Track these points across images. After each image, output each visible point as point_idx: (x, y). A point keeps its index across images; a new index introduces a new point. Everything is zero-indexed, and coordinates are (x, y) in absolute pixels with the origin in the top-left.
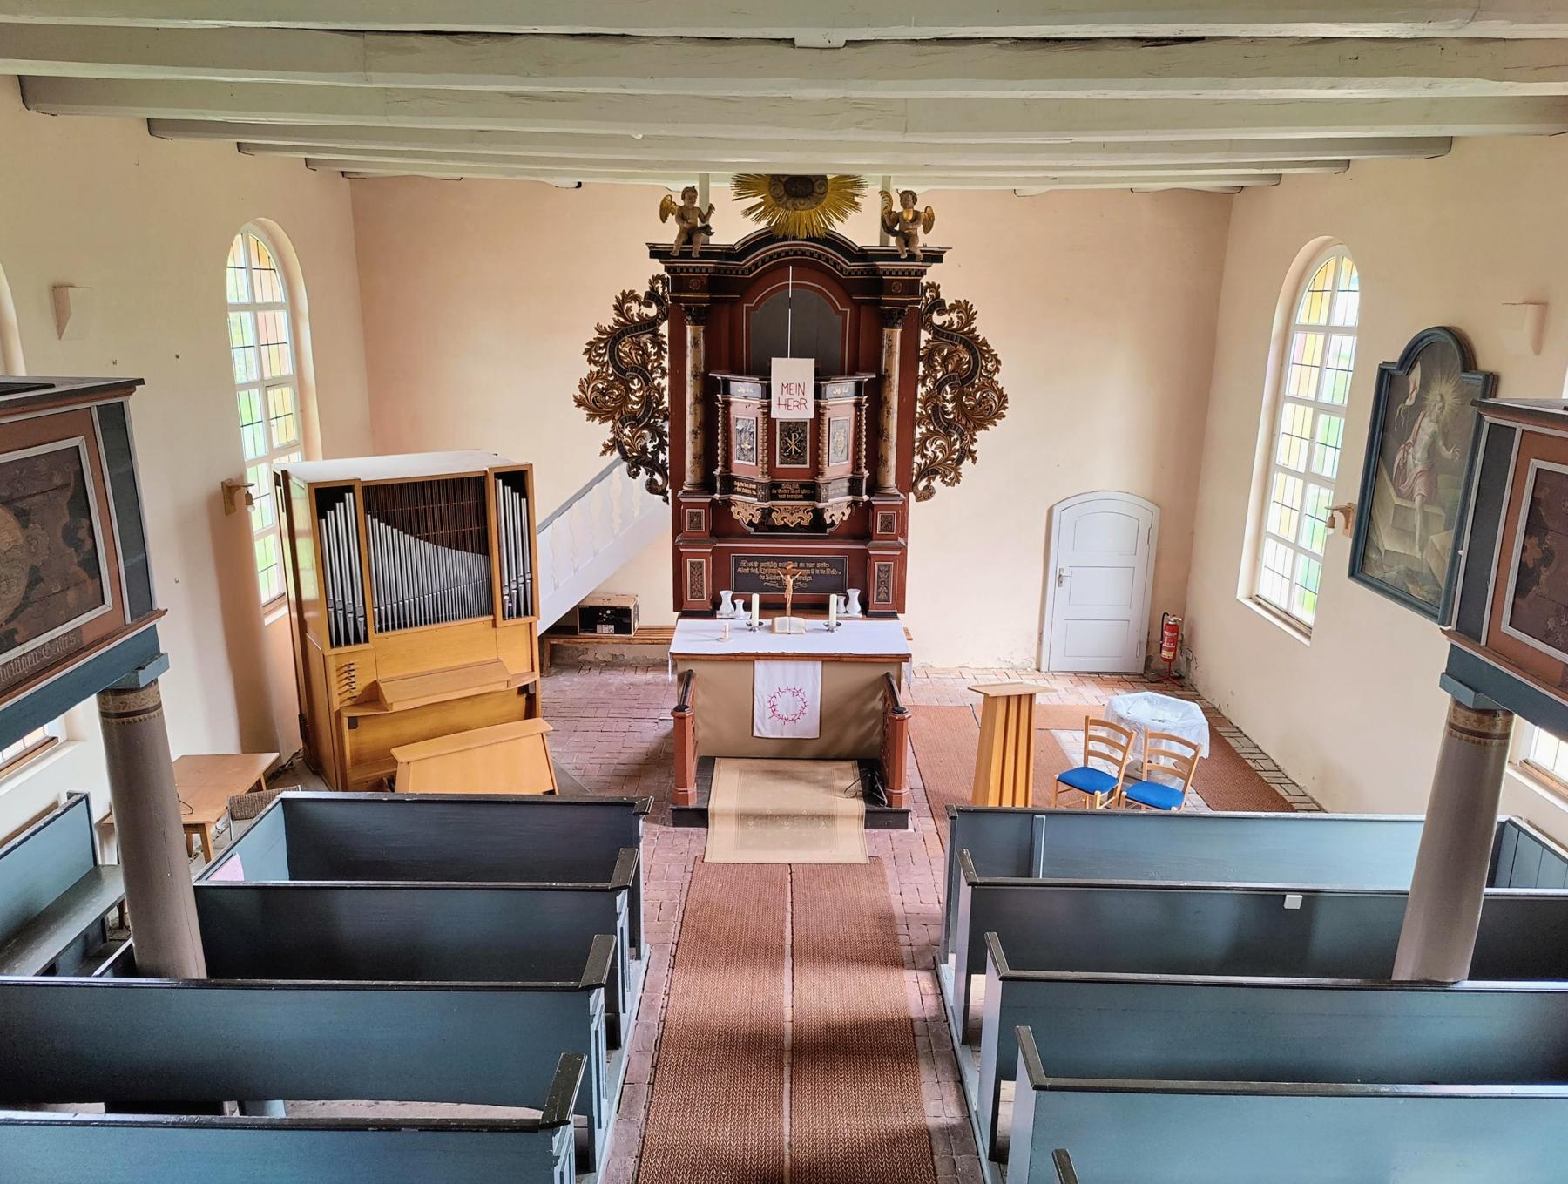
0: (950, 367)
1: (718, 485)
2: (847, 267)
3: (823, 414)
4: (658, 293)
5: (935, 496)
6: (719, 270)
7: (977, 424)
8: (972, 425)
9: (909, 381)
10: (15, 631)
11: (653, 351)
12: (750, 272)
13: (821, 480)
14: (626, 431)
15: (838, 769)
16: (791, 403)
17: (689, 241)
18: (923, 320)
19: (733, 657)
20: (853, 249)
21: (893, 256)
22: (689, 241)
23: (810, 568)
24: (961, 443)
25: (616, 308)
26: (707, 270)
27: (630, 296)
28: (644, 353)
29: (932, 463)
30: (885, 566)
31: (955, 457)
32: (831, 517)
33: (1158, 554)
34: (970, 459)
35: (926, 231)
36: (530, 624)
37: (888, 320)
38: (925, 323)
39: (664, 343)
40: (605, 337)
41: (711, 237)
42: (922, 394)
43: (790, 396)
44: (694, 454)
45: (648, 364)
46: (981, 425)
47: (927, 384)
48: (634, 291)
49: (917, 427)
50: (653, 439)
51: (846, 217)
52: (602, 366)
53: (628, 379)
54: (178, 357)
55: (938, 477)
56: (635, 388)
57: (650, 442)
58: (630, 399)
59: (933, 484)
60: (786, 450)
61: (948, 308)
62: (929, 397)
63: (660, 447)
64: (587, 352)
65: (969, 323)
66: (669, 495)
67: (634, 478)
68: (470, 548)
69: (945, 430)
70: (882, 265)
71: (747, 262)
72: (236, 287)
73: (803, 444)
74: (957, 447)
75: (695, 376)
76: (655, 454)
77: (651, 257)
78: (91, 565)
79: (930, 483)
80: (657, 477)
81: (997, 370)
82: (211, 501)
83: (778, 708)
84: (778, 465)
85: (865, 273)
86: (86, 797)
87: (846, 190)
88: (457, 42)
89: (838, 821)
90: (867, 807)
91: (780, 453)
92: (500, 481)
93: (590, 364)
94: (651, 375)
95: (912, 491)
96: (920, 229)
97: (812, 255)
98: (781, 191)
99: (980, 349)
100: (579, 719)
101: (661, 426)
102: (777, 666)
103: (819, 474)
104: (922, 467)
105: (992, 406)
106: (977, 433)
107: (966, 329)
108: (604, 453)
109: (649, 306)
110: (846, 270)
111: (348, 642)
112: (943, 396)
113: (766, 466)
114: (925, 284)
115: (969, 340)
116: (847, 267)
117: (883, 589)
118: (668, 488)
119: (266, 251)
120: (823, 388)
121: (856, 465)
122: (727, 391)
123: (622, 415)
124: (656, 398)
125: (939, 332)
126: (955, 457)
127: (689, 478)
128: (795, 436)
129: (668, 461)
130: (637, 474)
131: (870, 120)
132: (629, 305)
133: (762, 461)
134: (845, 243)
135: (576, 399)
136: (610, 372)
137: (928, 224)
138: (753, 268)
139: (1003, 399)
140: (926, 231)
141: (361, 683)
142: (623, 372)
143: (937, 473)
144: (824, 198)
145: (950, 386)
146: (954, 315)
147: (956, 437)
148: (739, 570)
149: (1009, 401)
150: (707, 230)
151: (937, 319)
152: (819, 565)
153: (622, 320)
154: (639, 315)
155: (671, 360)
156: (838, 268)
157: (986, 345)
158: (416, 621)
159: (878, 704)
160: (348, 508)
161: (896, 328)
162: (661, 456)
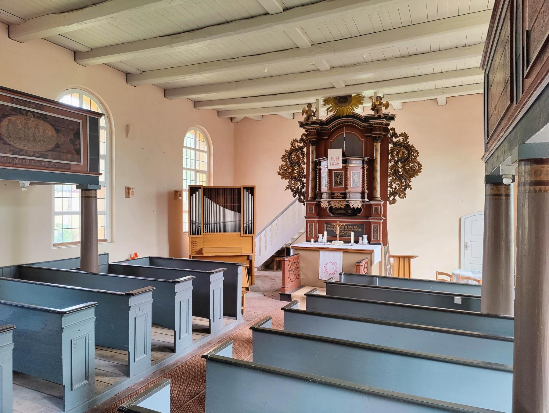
0: (400, 156)
3: (348, 168)
4: (303, 138)
6: (321, 130)
7: (411, 175)
8: (409, 175)
10: (48, 155)
11: (301, 157)
12: (331, 129)
13: (347, 191)
14: (293, 182)
16: (334, 163)
18: (389, 141)
19: (311, 249)
20: (363, 118)
24: (405, 182)
25: (291, 144)
27: (295, 140)
30: (376, 226)
34: (409, 188)
35: (386, 109)
36: (253, 236)
37: (375, 140)
38: (390, 141)
39: (305, 154)
40: (287, 153)
42: (390, 166)
44: (311, 188)
45: (300, 161)
47: (392, 162)
51: (358, 107)
52: (286, 162)
54: (164, 153)
55: (398, 195)
56: (296, 168)
57: (300, 185)
58: (294, 172)
59: (396, 198)
62: (393, 166)
63: (303, 187)
64: (282, 158)
65: (406, 140)
66: (305, 203)
67: (295, 197)
68: (237, 210)
70: (372, 121)
71: (330, 126)
74: (404, 184)
75: (312, 162)
78: (78, 152)
79: (395, 198)
80: (302, 198)
81: (418, 156)
83: (327, 269)
84: (333, 187)
85: (368, 126)
86: (108, 254)
87: (359, 99)
88: (190, 33)
92: (245, 190)
94: (301, 164)
97: (350, 122)
98: (337, 102)
99: (411, 149)
102: (327, 253)
103: (347, 189)
104: (391, 192)
106: (411, 179)
107: (405, 142)
108: (286, 190)
109: (301, 143)
110: (362, 126)
114: (390, 128)
119: (202, 137)
122: (320, 165)
125: (395, 144)
126: (403, 188)
130: (295, 196)
131: (323, 50)
132: (295, 143)
134: (359, 116)
135: (278, 173)
136: (289, 164)
137: (387, 106)
139: (420, 166)
140: (386, 109)
141: (199, 248)
146: (401, 138)
147: (403, 180)
149: (422, 166)
151: (394, 140)
152: (355, 227)
153: (293, 148)
157: (414, 147)
160: (200, 192)
162: (303, 190)
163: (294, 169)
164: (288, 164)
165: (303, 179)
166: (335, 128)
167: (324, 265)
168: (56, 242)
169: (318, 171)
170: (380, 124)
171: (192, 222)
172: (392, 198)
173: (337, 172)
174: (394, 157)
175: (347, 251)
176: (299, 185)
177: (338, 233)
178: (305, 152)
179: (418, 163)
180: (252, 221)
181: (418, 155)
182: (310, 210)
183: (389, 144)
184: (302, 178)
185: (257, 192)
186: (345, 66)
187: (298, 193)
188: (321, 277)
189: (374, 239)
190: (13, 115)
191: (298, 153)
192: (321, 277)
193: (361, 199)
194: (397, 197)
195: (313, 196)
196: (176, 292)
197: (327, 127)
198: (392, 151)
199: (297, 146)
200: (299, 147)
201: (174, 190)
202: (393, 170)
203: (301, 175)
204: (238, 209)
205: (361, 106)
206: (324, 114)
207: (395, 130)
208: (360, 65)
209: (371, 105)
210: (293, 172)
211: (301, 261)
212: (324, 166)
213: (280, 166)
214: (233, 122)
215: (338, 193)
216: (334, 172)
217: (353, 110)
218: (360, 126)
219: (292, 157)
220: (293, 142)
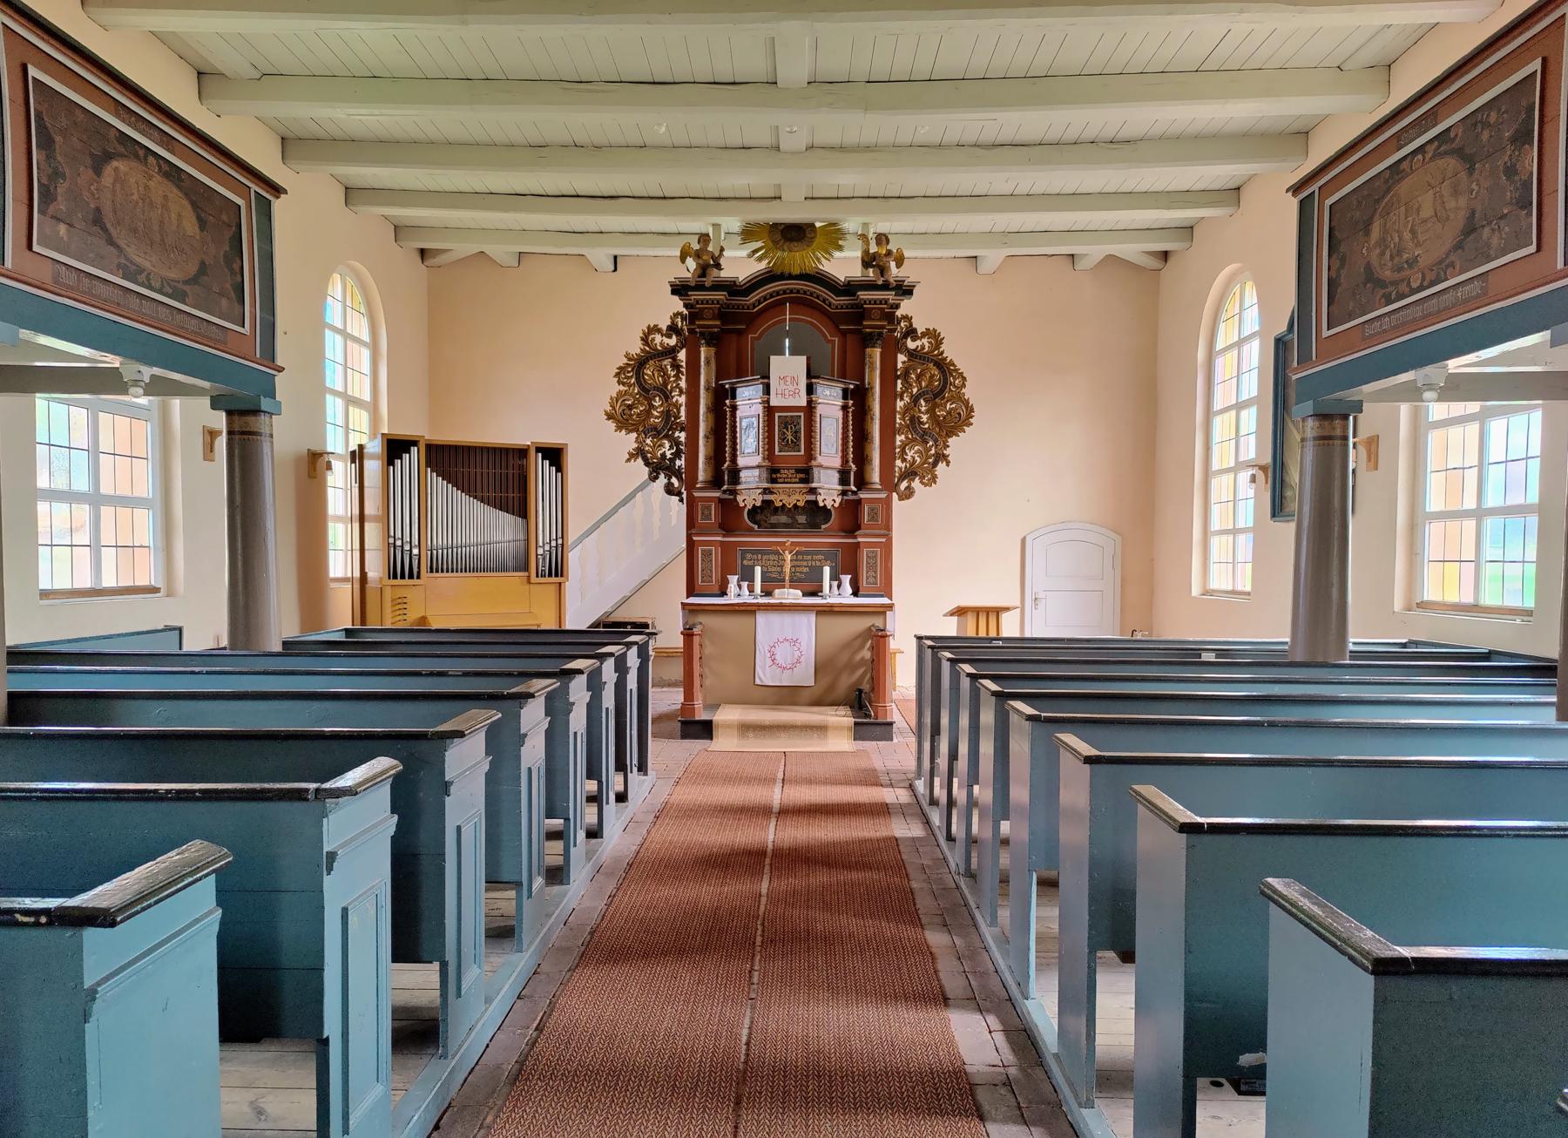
0: (923, 384)
1: (726, 478)
3: (815, 408)
9: (889, 396)
11: (673, 373)
12: (754, 307)
13: (813, 463)
14: (648, 441)
16: (787, 392)
17: (703, 275)
18: (899, 346)
19: (737, 608)
20: (839, 284)
21: (871, 286)
22: (703, 275)
24: (936, 448)
25: (642, 339)
26: (718, 301)
29: (911, 466)
31: (931, 460)
33: (1123, 579)
35: (899, 265)
36: (560, 583)
37: (867, 340)
39: (682, 366)
41: (722, 271)
42: (900, 407)
43: (785, 387)
45: (668, 385)
46: (952, 432)
48: (657, 325)
49: (897, 436)
50: (671, 447)
54: (285, 333)
56: (656, 404)
59: (913, 485)
60: (783, 440)
62: (907, 409)
63: (677, 455)
64: (617, 375)
66: (684, 496)
69: (922, 436)
70: (863, 295)
71: (753, 297)
72: (333, 313)
73: (798, 434)
74: (933, 452)
75: (707, 389)
76: (672, 460)
77: (672, 294)
80: (674, 481)
81: (964, 386)
82: (298, 460)
84: (777, 453)
86: (180, 630)
87: (833, 237)
89: (830, 733)
92: (540, 454)
94: (671, 393)
95: (896, 491)
96: (893, 264)
97: (805, 293)
98: (778, 236)
103: (812, 459)
105: (959, 414)
108: (628, 460)
109: (669, 337)
111: (403, 577)
113: (767, 453)
114: (900, 316)
118: (683, 490)
119: (359, 298)
120: (814, 386)
122: (734, 397)
125: (912, 355)
126: (931, 460)
127: (702, 474)
128: (791, 428)
129: (683, 466)
134: (832, 280)
135: (606, 414)
137: (900, 261)
139: (970, 410)
140: (899, 265)
142: (647, 391)
146: (925, 341)
147: (931, 443)
150: (718, 266)
151: (911, 345)
152: (815, 557)
153: (648, 349)
155: (686, 381)
156: (827, 302)
157: (954, 365)
158: (457, 569)
159: (866, 654)
160: (414, 456)
161: (876, 347)
162: (678, 463)
163: (652, 407)
164: (634, 390)
165: (677, 434)
166: (760, 306)
168: (44, 584)
170: (883, 302)
171: (391, 540)
172: (904, 485)
174: (911, 385)
176: (668, 448)
177: (787, 569)
179: (966, 403)
180: (560, 541)
183: (899, 355)
184: (676, 429)
185: (571, 461)
186: (842, 149)
188: (760, 679)
190: (122, 156)
192: (760, 679)
193: (840, 485)
194: (916, 484)
195: (708, 480)
196: (605, 683)
198: (906, 373)
199: (661, 343)
200: (666, 348)
201: (308, 450)
204: (519, 506)
205: (837, 254)
206: (740, 263)
207: (913, 321)
208: (878, 151)
209: (859, 254)
210: (648, 413)
214: (425, 263)
218: (830, 305)
219: (648, 375)
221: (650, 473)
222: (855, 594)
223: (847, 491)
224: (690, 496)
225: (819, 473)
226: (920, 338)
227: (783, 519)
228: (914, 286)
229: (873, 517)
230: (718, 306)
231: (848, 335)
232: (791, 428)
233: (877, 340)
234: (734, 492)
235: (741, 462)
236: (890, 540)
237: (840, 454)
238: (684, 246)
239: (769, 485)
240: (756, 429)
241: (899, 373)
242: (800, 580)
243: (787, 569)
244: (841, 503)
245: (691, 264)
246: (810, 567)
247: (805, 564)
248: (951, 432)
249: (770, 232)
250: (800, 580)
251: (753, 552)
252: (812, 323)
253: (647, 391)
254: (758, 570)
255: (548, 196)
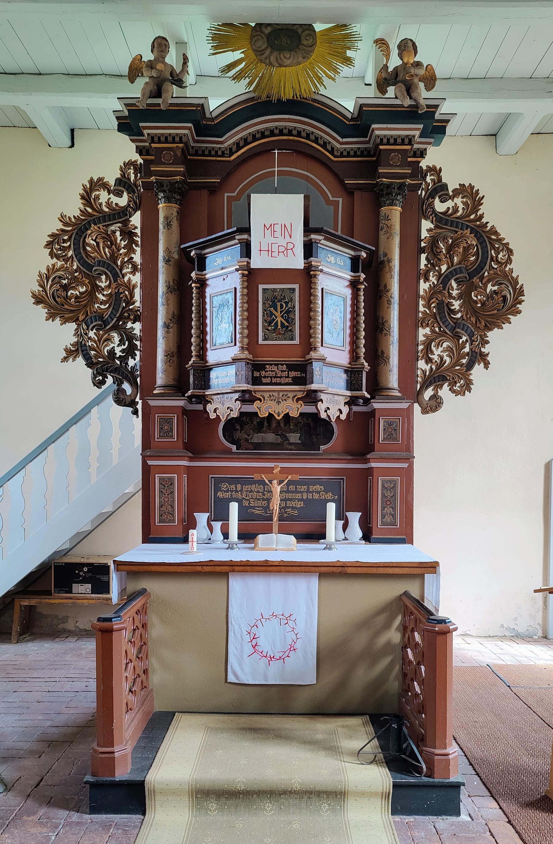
1: (191, 380)
2: (338, 146)
3: (315, 276)
4: (129, 179)
5: (444, 406)
6: (197, 151)
11: (123, 243)
12: (231, 154)
13: (313, 354)
14: (92, 334)
15: (343, 727)
16: (275, 248)
17: (158, 93)
19: (199, 568)
23: (302, 492)
25: (83, 197)
28: (112, 244)
29: (438, 368)
30: (391, 481)
31: (464, 361)
32: (326, 411)
34: (482, 365)
38: (426, 209)
39: (135, 235)
40: (70, 228)
42: (425, 290)
44: (166, 351)
47: (431, 278)
50: (121, 342)
53: (94, 274)
56: (103, 285)
57: (119, 345)
58: (97, 298)
59: (440, 393)
60: (270, 323)
61: (451, 194)
62: (433, 292)
64: (49, 245)
66: (139, 407)
69: (453, 330)
73: (291, 316)
74: (467, 350)
75: (167, 261)
80: (127, 387)
84: (261, 342)
90: (394, 778)
91: (264, 326)
93: (52, 258)
94: (121, 270)
95: (418, 402)
98: (262, 44)
99: (489, 238)
100: (27, 679)
101: (132, 328)
103: (311, 350)
104: (427, 374)
105: (505, 297)
107: (472, 217)
108: (65, 359)
109: (119, 194)
110: (338, 150)
112: (449, 292)
114: (425, 168)
115: (476, 228)
116: (338, 146)
117: (388, 510)
121: (354, 356)
122: (202, 267)
123: (87, 315)
124: (126, 296)
126: (464, 361)
128: (282, 306)
129: (138, 368)
130: (103, 382)
132: (97, 193)
133: (242, 307)
135: (34, 296)
138: (234, 149)
143: (444, 379)
144: (312, 51)
145: (455, 280)
146: (458, 201)
147: (464, 338)
148: (220, 494)
150: (179, 82)
151: (440, 207)
152: (312, 488)
153: (90, 210)
154: (109, 204)
155: (142, 254)
157: (496, 233)
162: (131, 363)
163: (95, 288)
165: (129, 325)
167: (245, 628)
169: (194, 291)
173: (274, 290)
175: (339, 570)
176: (117, 344)
177: (276, 505)
178: (136, 228)
181: (509, 257)
182: (161, 428)
183: (424, 222)
184: (128, 318)
187: (110, 372)
189: (383, 524)
191: (113, 228)
194: (445, 392)
195: (171, 382)
197: (221, 143)
198: (433, 242)
200: (114, 210)
202: (433, 305)
203: (124, 308)
205: (345, 71)
211: (154, 619)
212: (222, 269)
213: (44, 271)
215: (275, 365)
216: (264, 290)
217: (321, 83)
218: (332, 152)
220: (92, 189)
221: (94, 377)
222: (367, 537)
223: (357, 397)
224: (145, 406)
225: (321, 370)
226: (452, 198)
227: (270, 437)
228: (448, 121)
229: (391, 435)
230: (181, 145)
231: (357, 194)
232: (282, 306)
233: (397, 194)
234: (204, 400)
235: (212, 357)
236: (411, 468)
237: (348, 348)
238: (134, 59)
239: (250, 387)
240: (232, 309)
241: (423, 244)
242: (291, 518)
243: (276, 505)
244: (348, 414)
245: (141, 82)
246: (306, 501)
247: (299, 496)
248: (490, 323)
249: (252, 37)
250: (291, 518)
251: (232, 481)
252: (307, 178)
253: (90, 267)
254: (234, 507)
255: (6, 73)
